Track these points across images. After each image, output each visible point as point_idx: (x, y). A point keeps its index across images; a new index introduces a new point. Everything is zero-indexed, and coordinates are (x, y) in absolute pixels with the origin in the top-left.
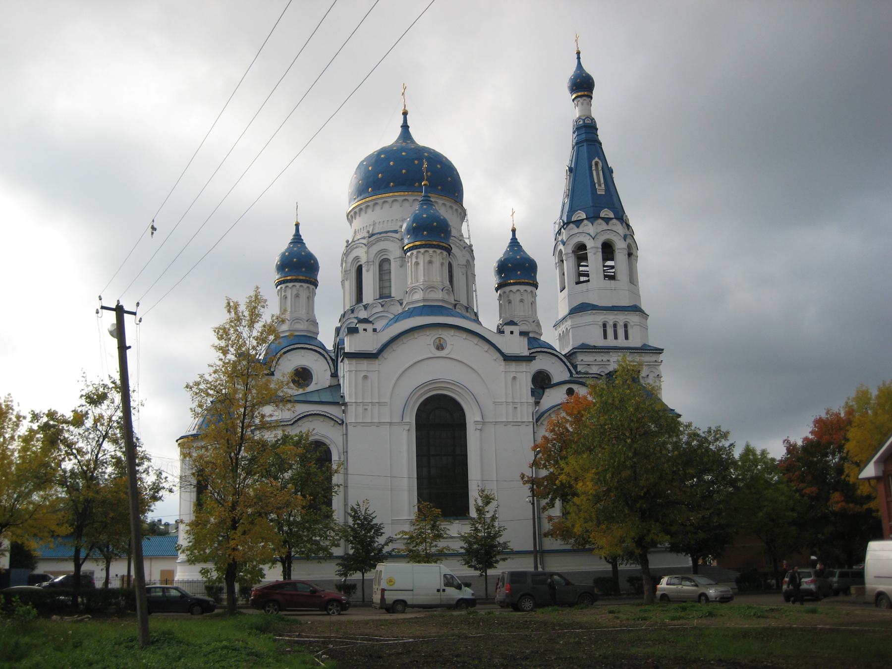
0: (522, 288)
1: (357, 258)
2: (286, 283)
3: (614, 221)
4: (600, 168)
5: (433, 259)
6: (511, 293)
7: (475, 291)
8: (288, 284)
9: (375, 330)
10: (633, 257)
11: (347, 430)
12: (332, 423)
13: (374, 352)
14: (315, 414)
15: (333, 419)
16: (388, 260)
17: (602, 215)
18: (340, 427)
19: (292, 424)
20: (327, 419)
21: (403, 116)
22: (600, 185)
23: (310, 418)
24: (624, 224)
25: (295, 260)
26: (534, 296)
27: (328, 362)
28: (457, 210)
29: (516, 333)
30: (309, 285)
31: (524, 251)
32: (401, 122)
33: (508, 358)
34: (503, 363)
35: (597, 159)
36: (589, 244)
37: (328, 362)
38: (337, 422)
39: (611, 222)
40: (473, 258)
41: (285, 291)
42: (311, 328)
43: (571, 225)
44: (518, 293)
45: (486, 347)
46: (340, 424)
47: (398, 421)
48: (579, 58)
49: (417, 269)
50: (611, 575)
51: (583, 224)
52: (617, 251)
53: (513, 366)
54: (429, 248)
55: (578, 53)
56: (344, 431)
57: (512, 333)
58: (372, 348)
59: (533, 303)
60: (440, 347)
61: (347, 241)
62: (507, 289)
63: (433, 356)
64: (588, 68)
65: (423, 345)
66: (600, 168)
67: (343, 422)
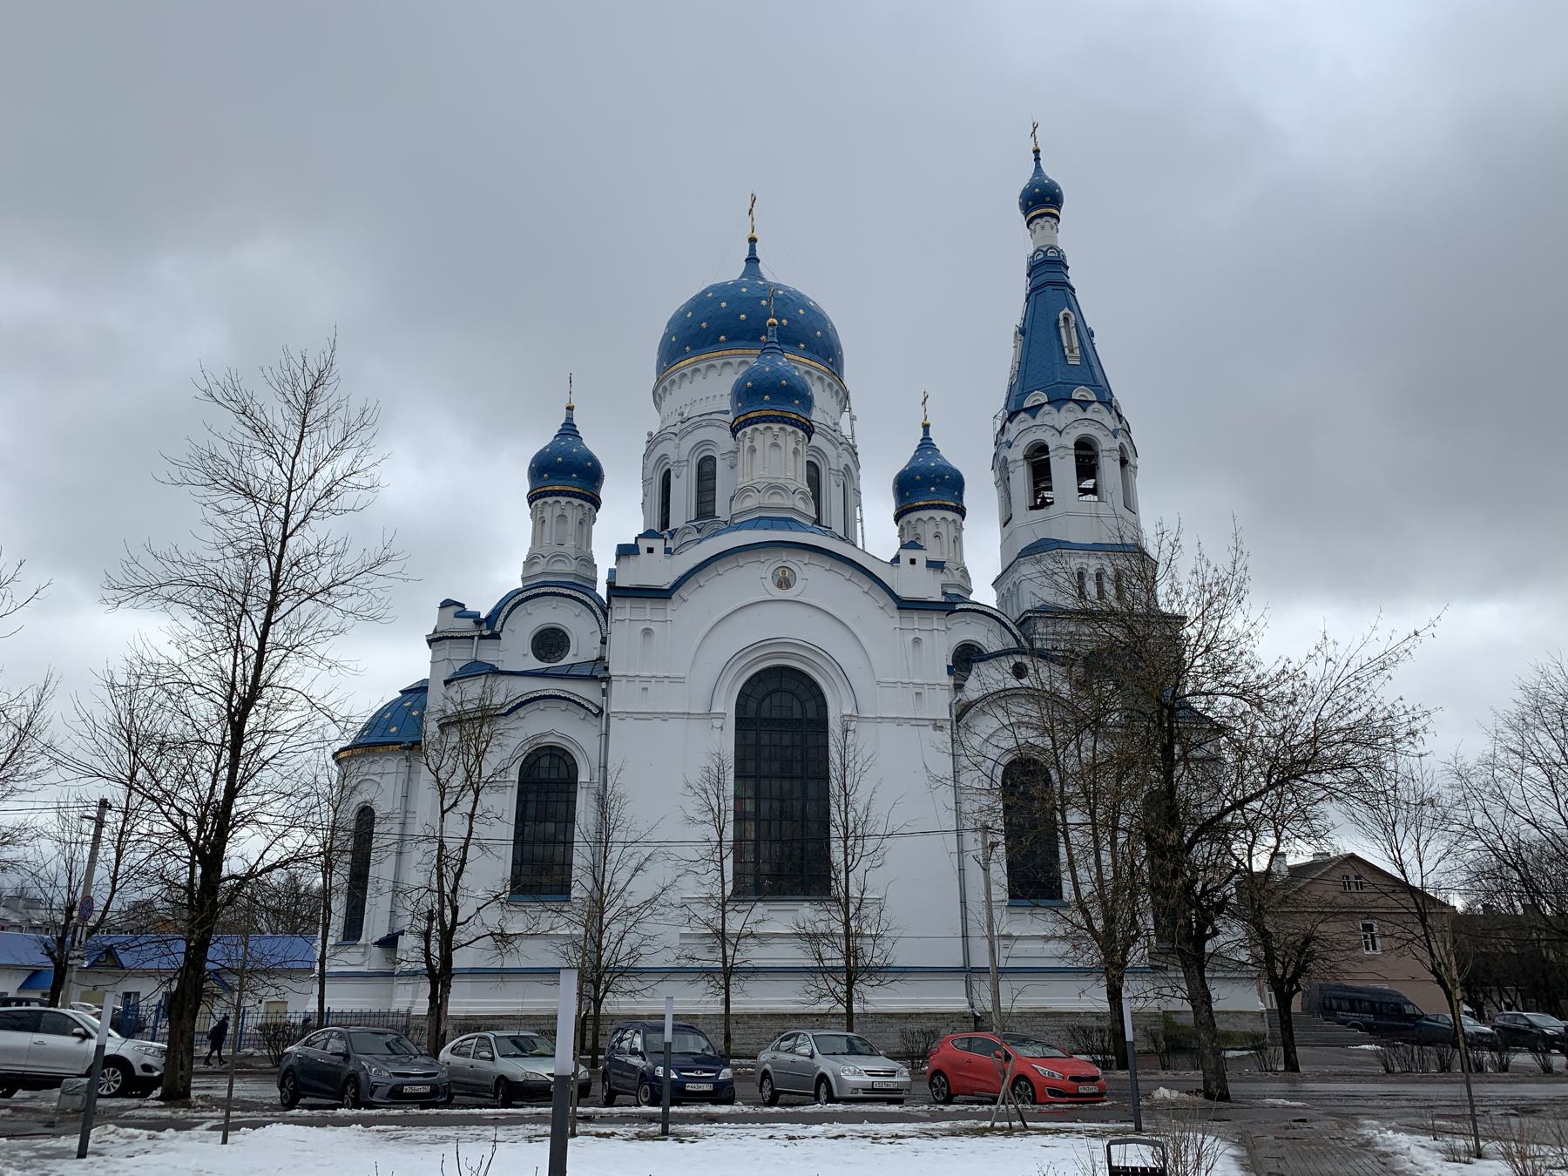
0: (938, 514)
1: (664, 457)
2: (544, 497)
3: (1096, 405)
4: (1072, 325)
5: (780, 442)
6: (920, 523)
7: (861, 520)
8: (547, 499)
9: (668, 551)
10: (1128, 468)
11: (608, 726)
12: (583, 713)
13: (667, 587)
14: (551, 697)
15: (583, 706)
16: (712, 459)
17: (1075, 396)
18: (596, 721)
19: (506, 714)
20: (572, 706)
21: (748, 245)
22: (1071, 351)
23: (541, 704)
24: (1114, 412)
25: (560, 459)
26: (960, 529)
27: (597, 619)
28: (830, 386)
29: (921, 563)
30: (584, 503)
31: (941, 457)
32: (746, 254)
33: (907, 605)
34: (896, 613)
35: (1066, 310)
36: (1052, 441)
37: (597, 619)
38: (590, 711)
39: (1090, 408)
40: (858, 467)
41: (542, 512)
42: (588, 574)
43: (1022, 415)
44: (932, 523)
45: (867, 584)
46: (596, 715)
47: (703, 712)
48: (1037, 159)
49: (752, 459)
50: (1106, 1024)
51: (1042, 411)
52: (1100, 455)
53: (916, 620)
54: (771, 422)
55: (1037, 152)
56: (604, 729)
57: (913, 562)
58: (664, 580)
59: (957, 540)
60: (784, 583)
61: (650, 434)
62: (913, 516)
63: (768, 597)
64: (1051, 172)
65: (754, 578)
66: (1072, 325)
67: (601, 711)
